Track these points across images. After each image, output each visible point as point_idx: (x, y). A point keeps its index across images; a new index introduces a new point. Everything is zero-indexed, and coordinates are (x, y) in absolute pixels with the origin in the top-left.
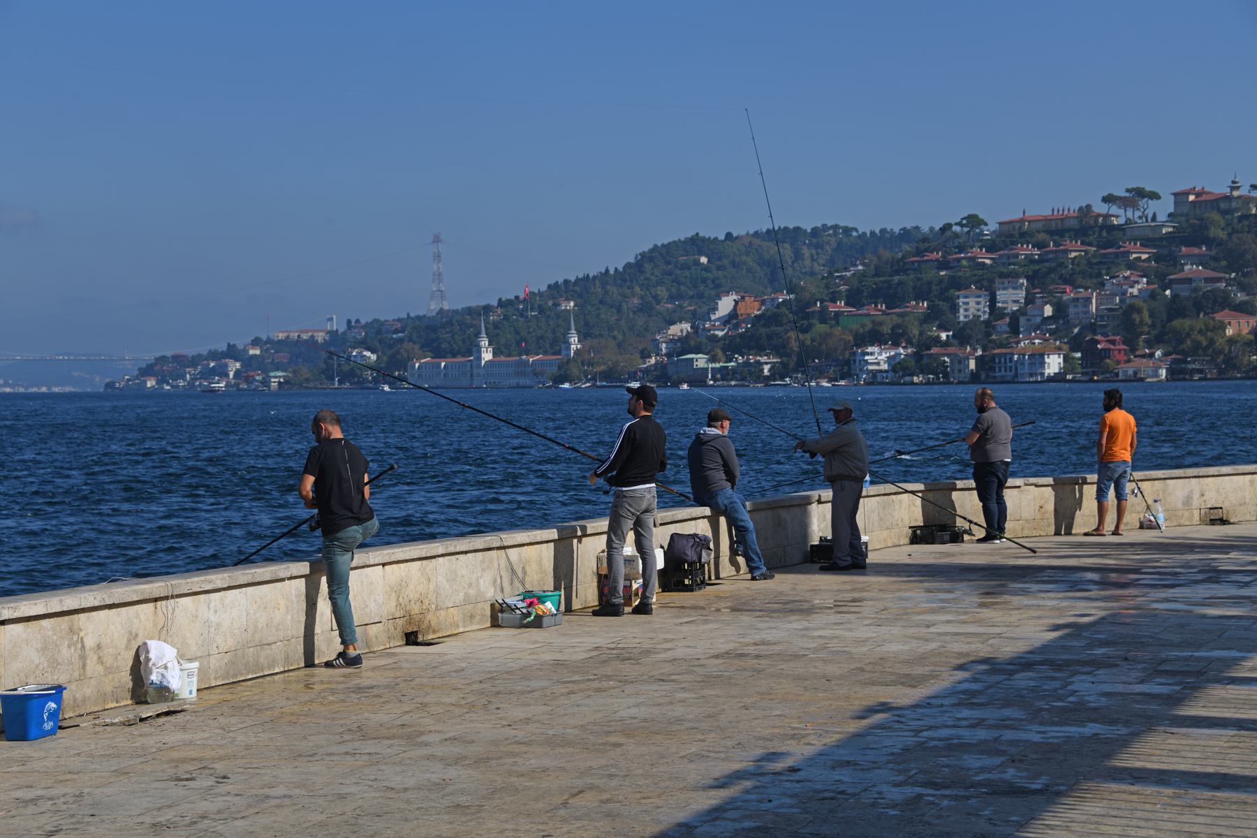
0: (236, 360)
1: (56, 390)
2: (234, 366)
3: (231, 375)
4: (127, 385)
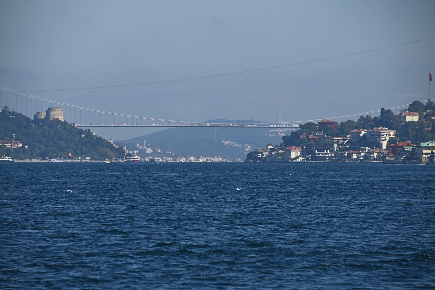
0: (390, 129)
1: (193, 160)
2: (387, 135)
3: (384, 144)
4: (270, 156)
